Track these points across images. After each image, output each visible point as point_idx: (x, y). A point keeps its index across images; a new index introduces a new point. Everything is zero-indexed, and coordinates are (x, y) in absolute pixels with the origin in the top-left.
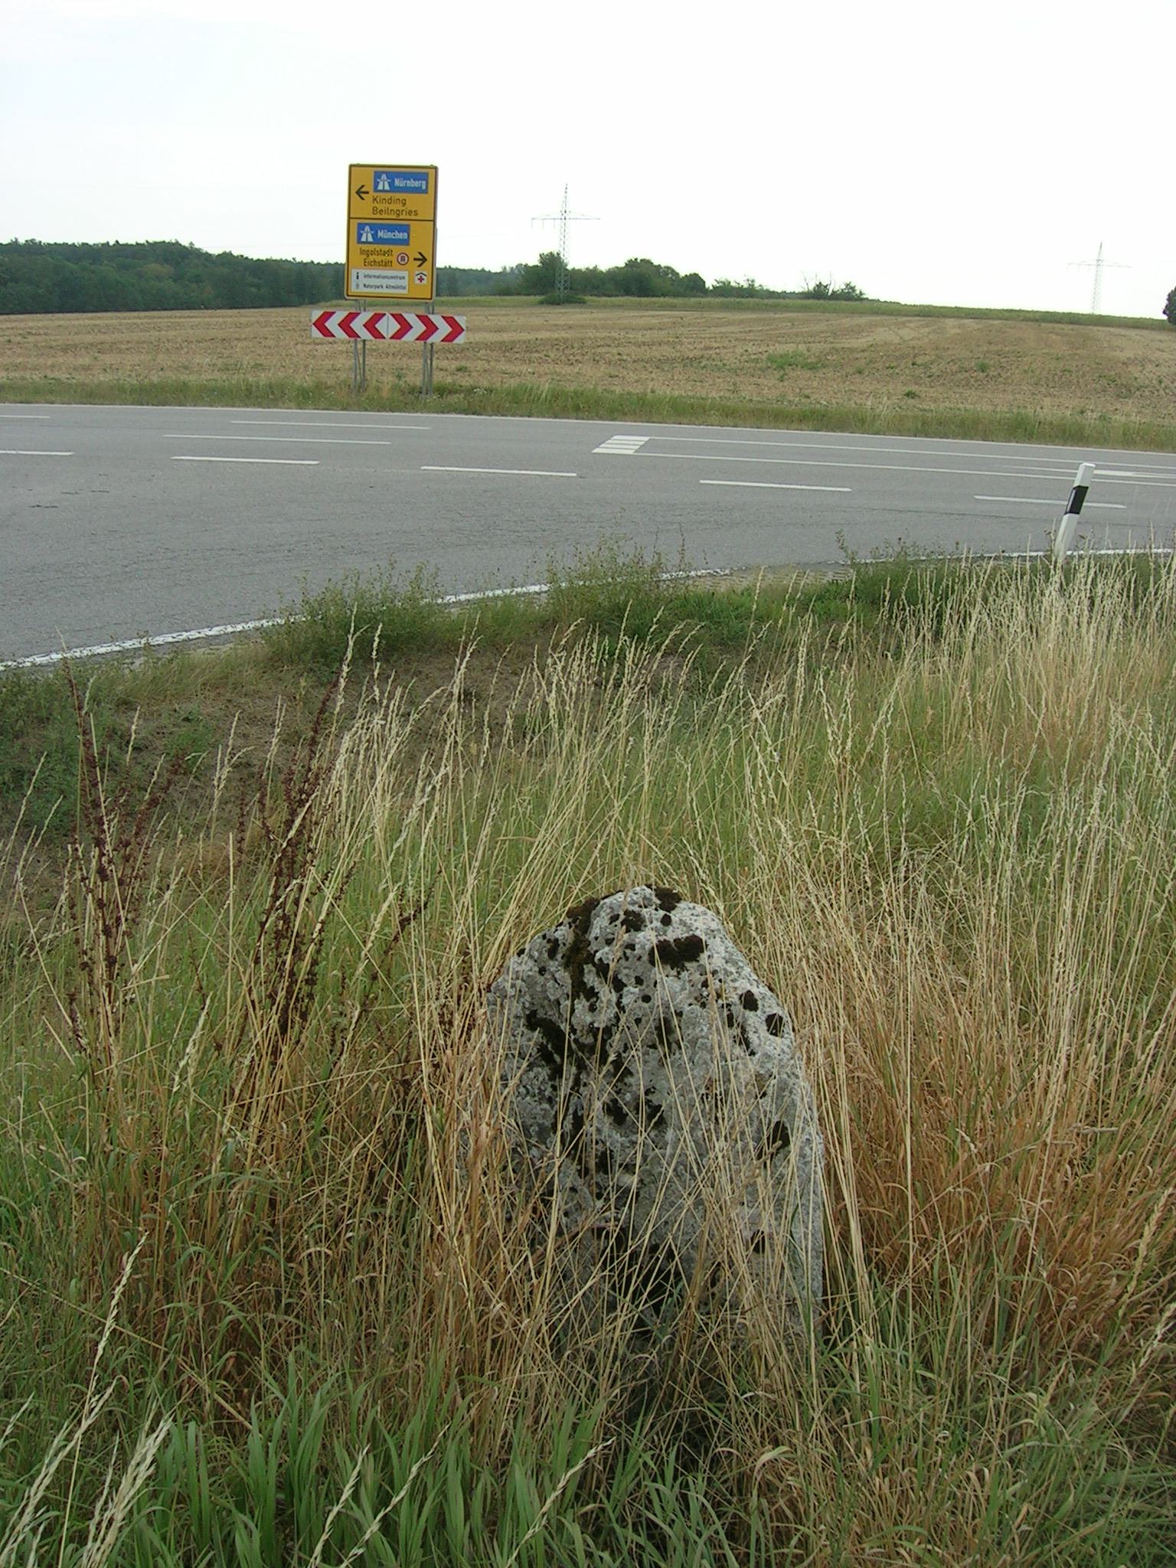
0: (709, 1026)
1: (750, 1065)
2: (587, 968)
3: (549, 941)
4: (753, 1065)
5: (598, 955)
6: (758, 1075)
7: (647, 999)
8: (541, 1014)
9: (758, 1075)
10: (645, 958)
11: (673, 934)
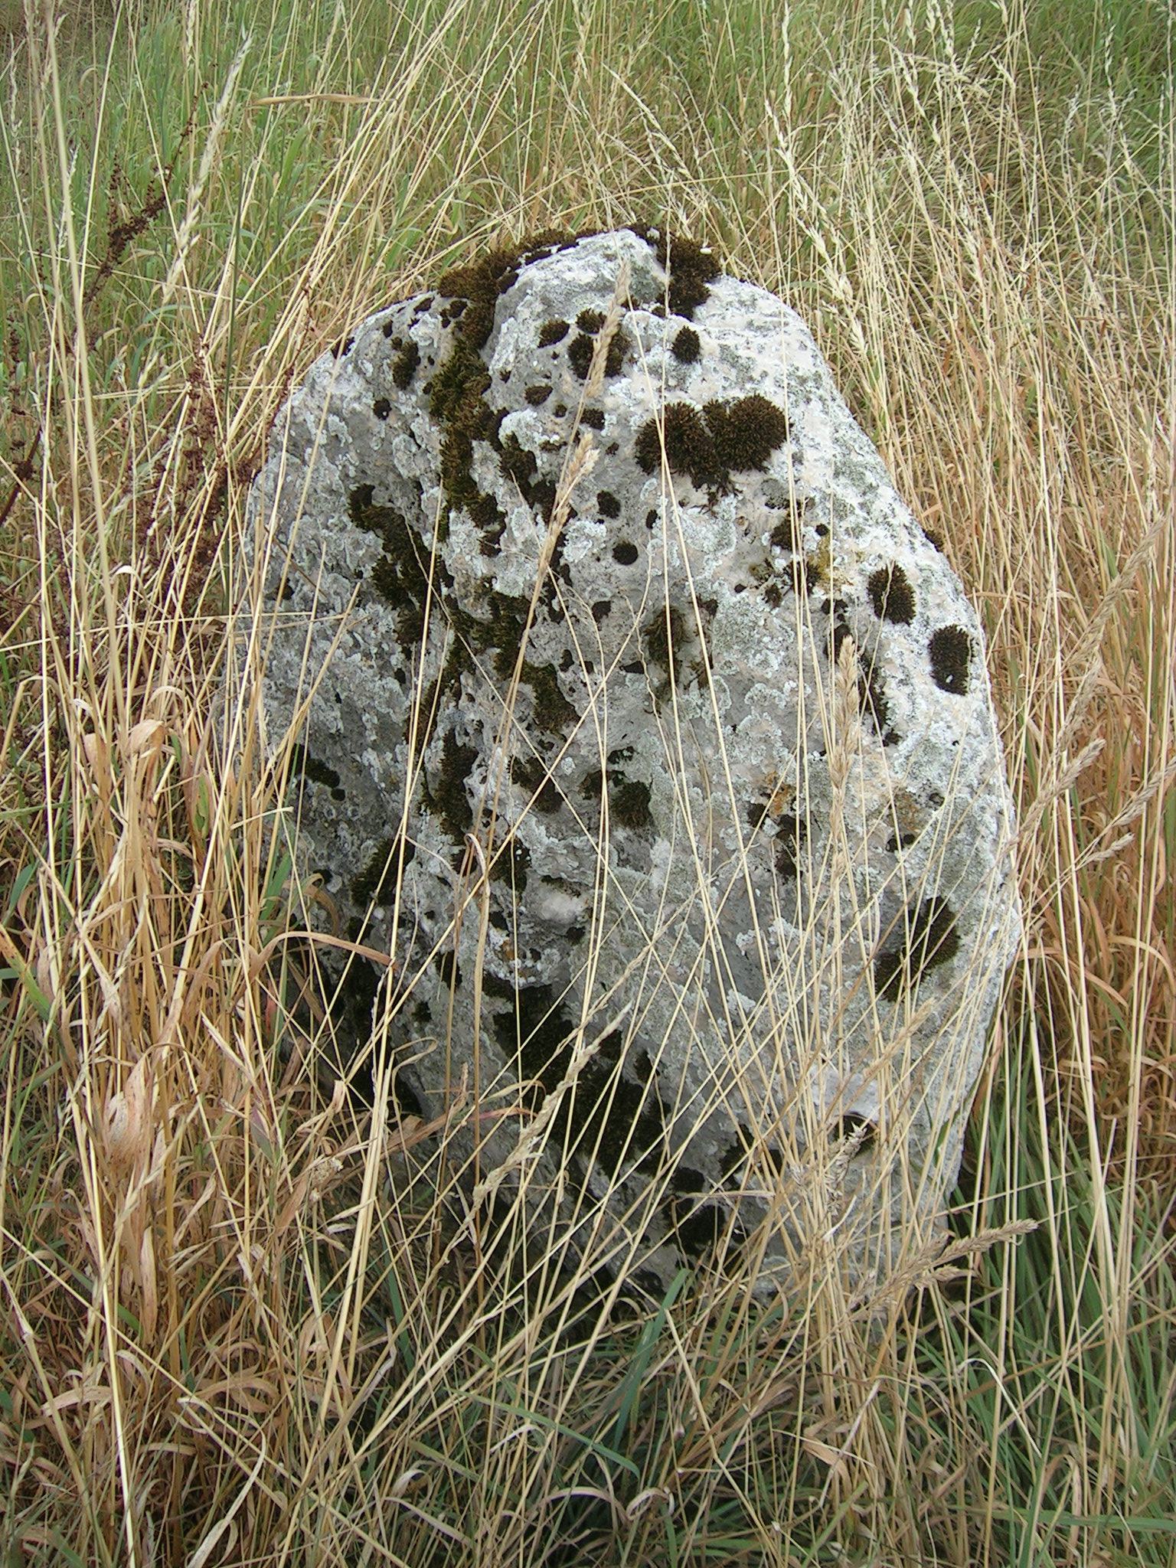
0: (777, 648)
1: (885, 772)
2: (481, 449)
3: (397, 344)
4: (890, 772)
5: (508, 426)
6: (901, 795)
7: (626, 554)
8: (379, 499)
9: (901, 795)
10: (628, 450)
11: (706, 387)
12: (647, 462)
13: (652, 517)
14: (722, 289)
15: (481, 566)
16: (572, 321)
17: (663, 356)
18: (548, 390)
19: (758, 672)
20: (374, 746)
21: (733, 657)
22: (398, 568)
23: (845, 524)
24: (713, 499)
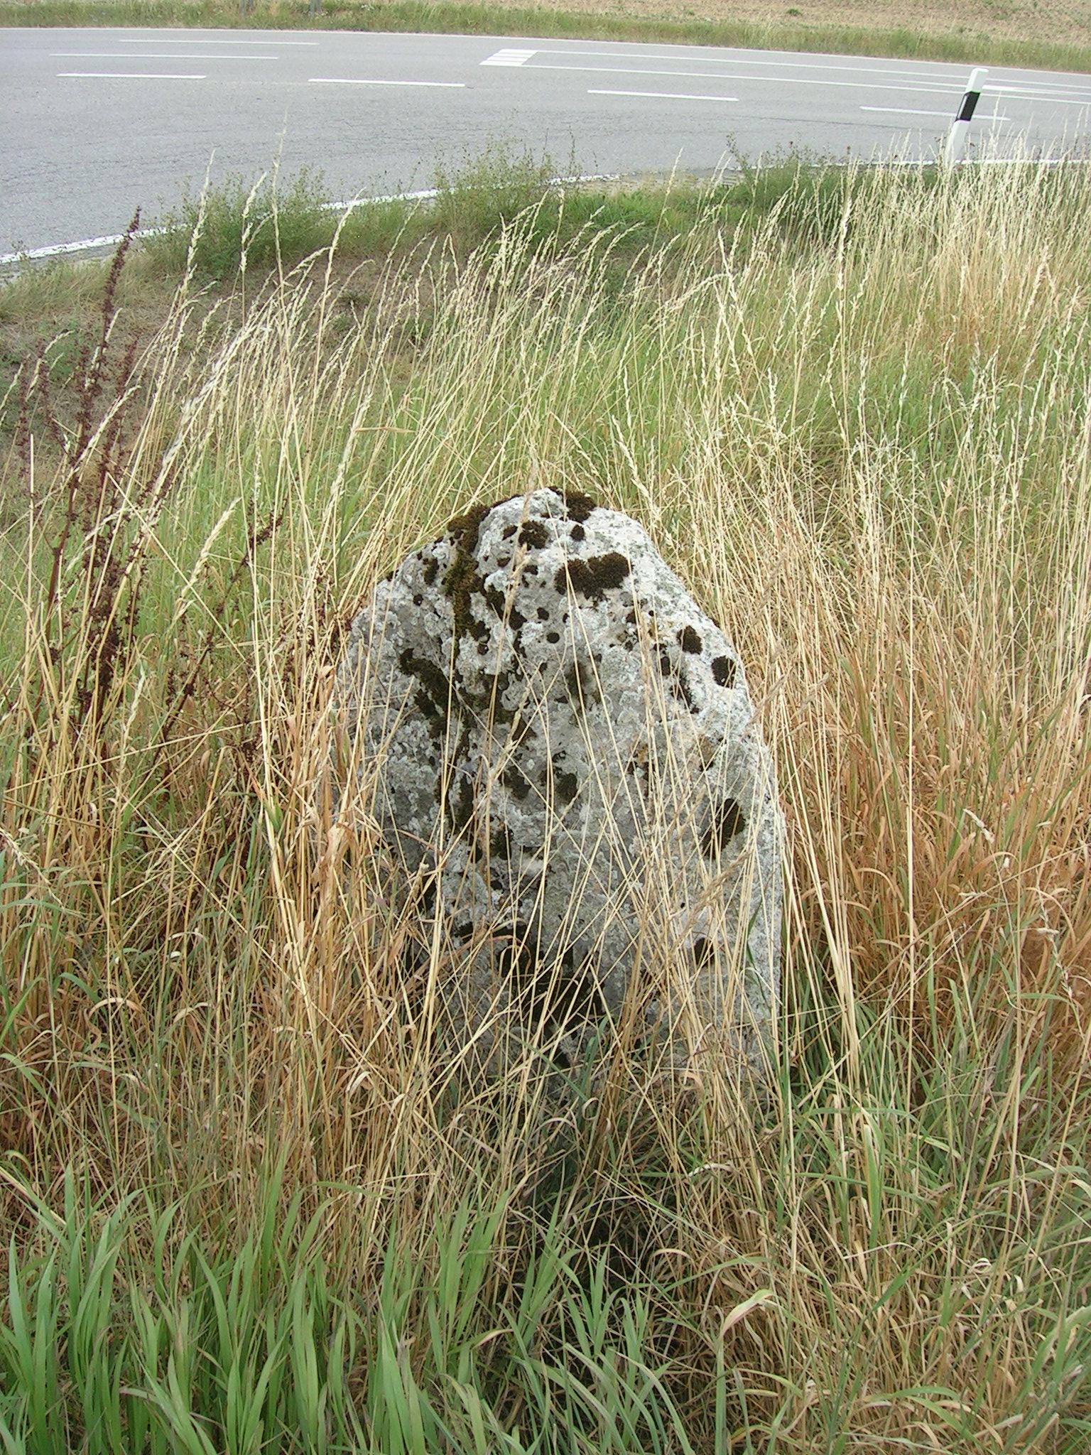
0: (635, 673)
1: (693, 727)
2: (475, 597)
3: (426, 561)
4: (696, 727)
5: (489, 581)
7: (553, 638)
8: (417, 654)
10: (551, 584)
11: (588, 551)
12: (561, 589)
13: (566, 616)
14: (598, 513)
15: (477, 663)
16: (519, 525)
17: (567, 539)
18: (509, 559)
19: (624, 685)
20: (417, 815)
21: (611, 681)
22: (429, 695)
23: (664, 610)
24: (595, 603)
